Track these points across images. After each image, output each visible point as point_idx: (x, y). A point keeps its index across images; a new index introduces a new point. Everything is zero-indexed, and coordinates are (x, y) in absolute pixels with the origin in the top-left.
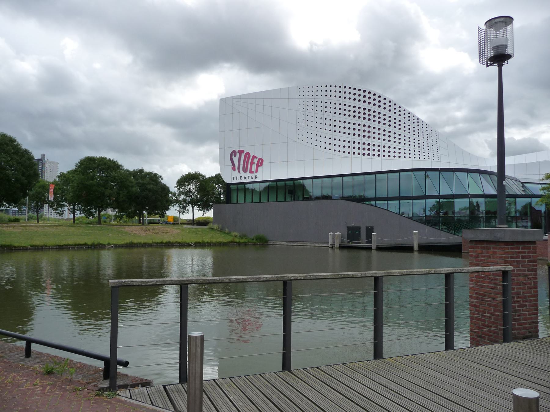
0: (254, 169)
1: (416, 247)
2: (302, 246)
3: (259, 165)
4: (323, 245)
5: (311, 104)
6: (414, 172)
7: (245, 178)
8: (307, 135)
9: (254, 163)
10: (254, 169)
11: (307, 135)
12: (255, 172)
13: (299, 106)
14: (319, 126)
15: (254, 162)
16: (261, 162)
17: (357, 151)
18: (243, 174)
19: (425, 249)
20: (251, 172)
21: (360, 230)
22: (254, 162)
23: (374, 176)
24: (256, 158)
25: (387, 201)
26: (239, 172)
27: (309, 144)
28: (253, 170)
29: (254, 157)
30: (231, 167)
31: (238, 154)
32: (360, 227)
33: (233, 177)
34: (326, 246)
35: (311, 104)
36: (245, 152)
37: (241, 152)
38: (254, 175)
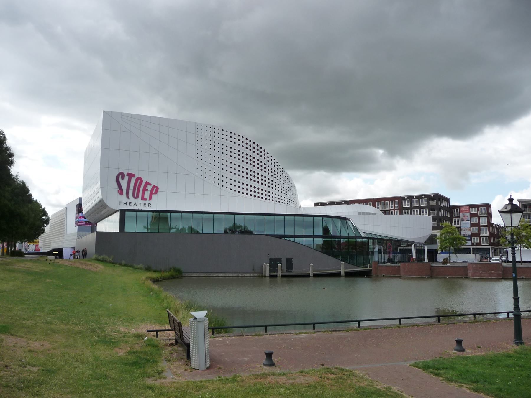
0: (147, 195)
1: (343, 273)
2: (196, 277)
3: (154, 192)
4: (246, 275)
5: (209, 143)
6: (324, 218)
7: (135, 204)
8: (206, 171)
9: (147, 190)
10: (147, 195)
11: (206, 171)
12: (148, 199)
13: (197, 142)
14: (217, 165)
15: (147, 188)
16: (155, 190)
17: (249, 193)
18: (132, 200)
19: (349, 275)
20: (143, 199)
21: (293, 261)
22: (147, 188)
23: (312, 218)
24: (150, 184)
25: (294, 238)
26: (128, 197)
27: (207, 180)
28: (145, 197)
29: (147, 184)
30: (117, 191)
31: (127, 178)
32: (282, 259)
33: (120, 202)
34: (250, 275)
35: (209, 143)
36: (136, 176)
37: (131, 176)
38: (147, 202)
